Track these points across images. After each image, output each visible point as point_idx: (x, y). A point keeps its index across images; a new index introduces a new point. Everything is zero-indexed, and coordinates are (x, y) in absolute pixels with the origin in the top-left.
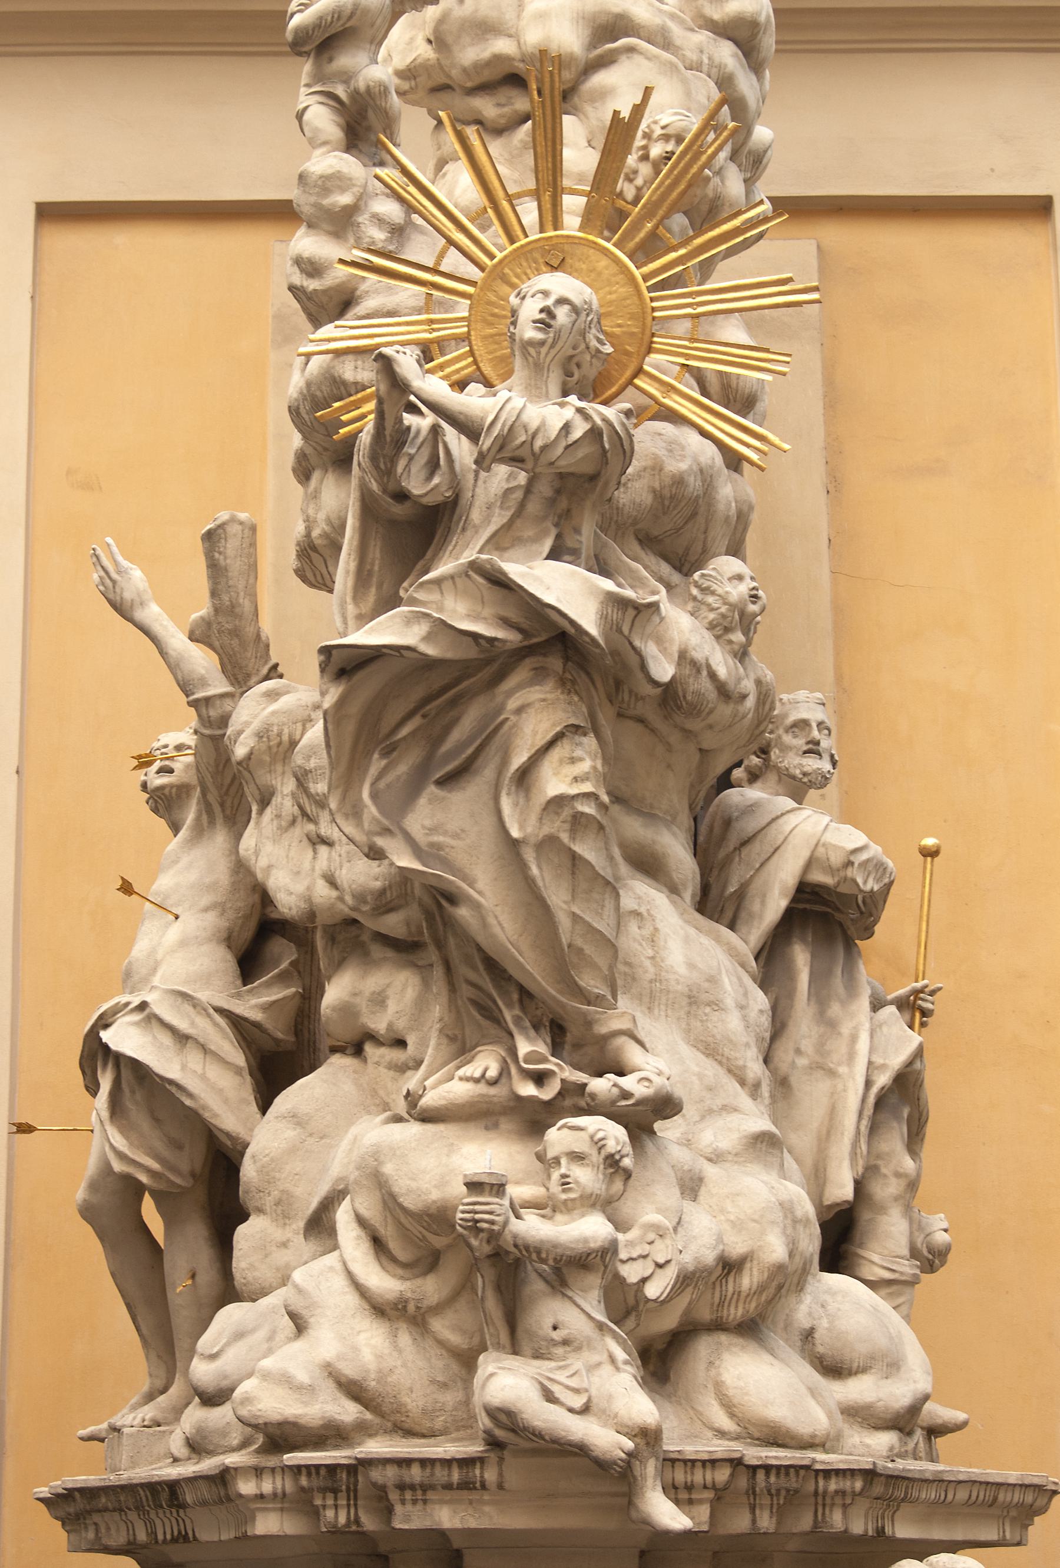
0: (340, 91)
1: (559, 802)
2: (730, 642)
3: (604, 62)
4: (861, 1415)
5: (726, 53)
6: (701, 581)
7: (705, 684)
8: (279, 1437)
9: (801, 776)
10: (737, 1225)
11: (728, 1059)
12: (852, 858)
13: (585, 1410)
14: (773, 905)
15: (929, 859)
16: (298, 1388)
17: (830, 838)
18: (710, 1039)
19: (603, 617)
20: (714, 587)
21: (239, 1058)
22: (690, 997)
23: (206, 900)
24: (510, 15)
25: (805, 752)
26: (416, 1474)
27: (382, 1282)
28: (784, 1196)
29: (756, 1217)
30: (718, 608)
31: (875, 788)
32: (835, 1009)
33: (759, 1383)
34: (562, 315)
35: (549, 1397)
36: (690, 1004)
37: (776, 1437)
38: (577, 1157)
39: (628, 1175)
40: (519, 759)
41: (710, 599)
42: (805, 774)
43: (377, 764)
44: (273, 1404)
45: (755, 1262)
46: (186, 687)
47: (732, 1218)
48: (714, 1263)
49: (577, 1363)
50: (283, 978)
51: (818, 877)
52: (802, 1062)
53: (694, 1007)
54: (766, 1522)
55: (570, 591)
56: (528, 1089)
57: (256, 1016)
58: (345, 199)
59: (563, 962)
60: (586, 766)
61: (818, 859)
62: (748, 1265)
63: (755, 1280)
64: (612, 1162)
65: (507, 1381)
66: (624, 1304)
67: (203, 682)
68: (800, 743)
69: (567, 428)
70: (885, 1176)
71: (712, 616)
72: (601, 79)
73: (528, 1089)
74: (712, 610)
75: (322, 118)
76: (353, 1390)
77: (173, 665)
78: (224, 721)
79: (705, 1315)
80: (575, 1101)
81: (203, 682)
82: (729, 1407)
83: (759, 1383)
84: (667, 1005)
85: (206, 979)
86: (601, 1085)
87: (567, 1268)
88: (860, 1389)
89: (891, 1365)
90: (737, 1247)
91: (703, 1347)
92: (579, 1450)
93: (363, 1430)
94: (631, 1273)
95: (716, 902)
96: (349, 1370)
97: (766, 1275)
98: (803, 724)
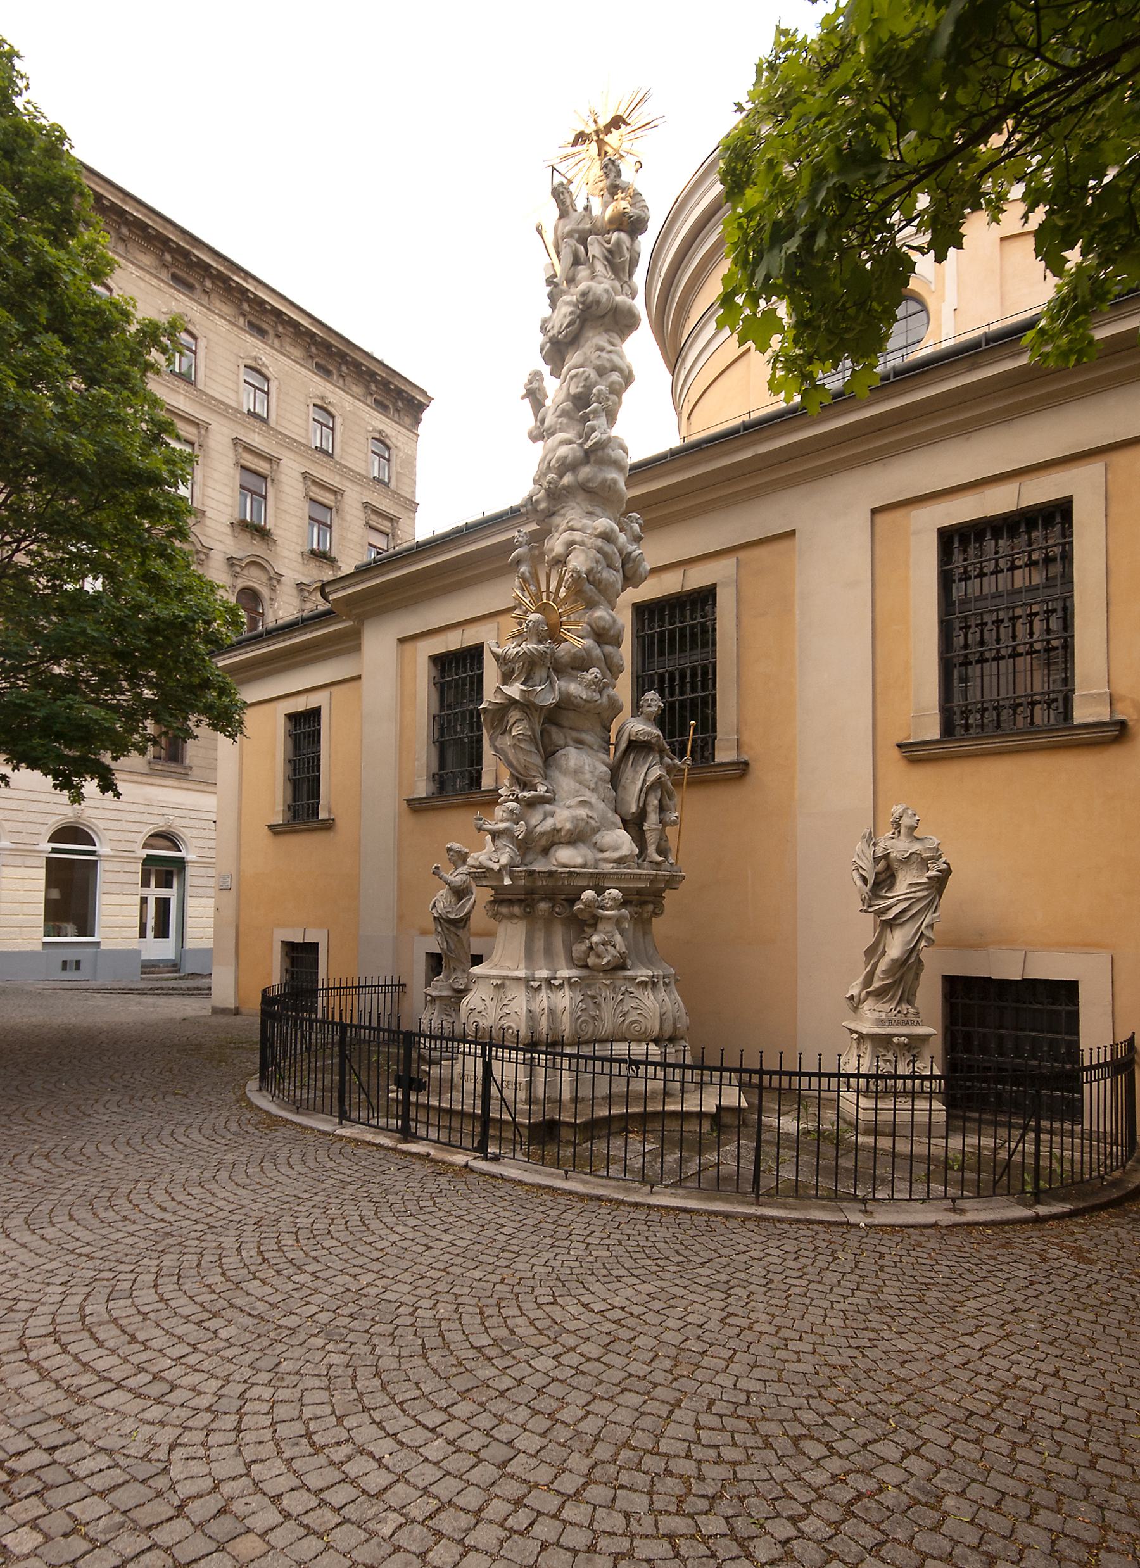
83: (567, 856)
88: (607, 855)
90: (559, 826)
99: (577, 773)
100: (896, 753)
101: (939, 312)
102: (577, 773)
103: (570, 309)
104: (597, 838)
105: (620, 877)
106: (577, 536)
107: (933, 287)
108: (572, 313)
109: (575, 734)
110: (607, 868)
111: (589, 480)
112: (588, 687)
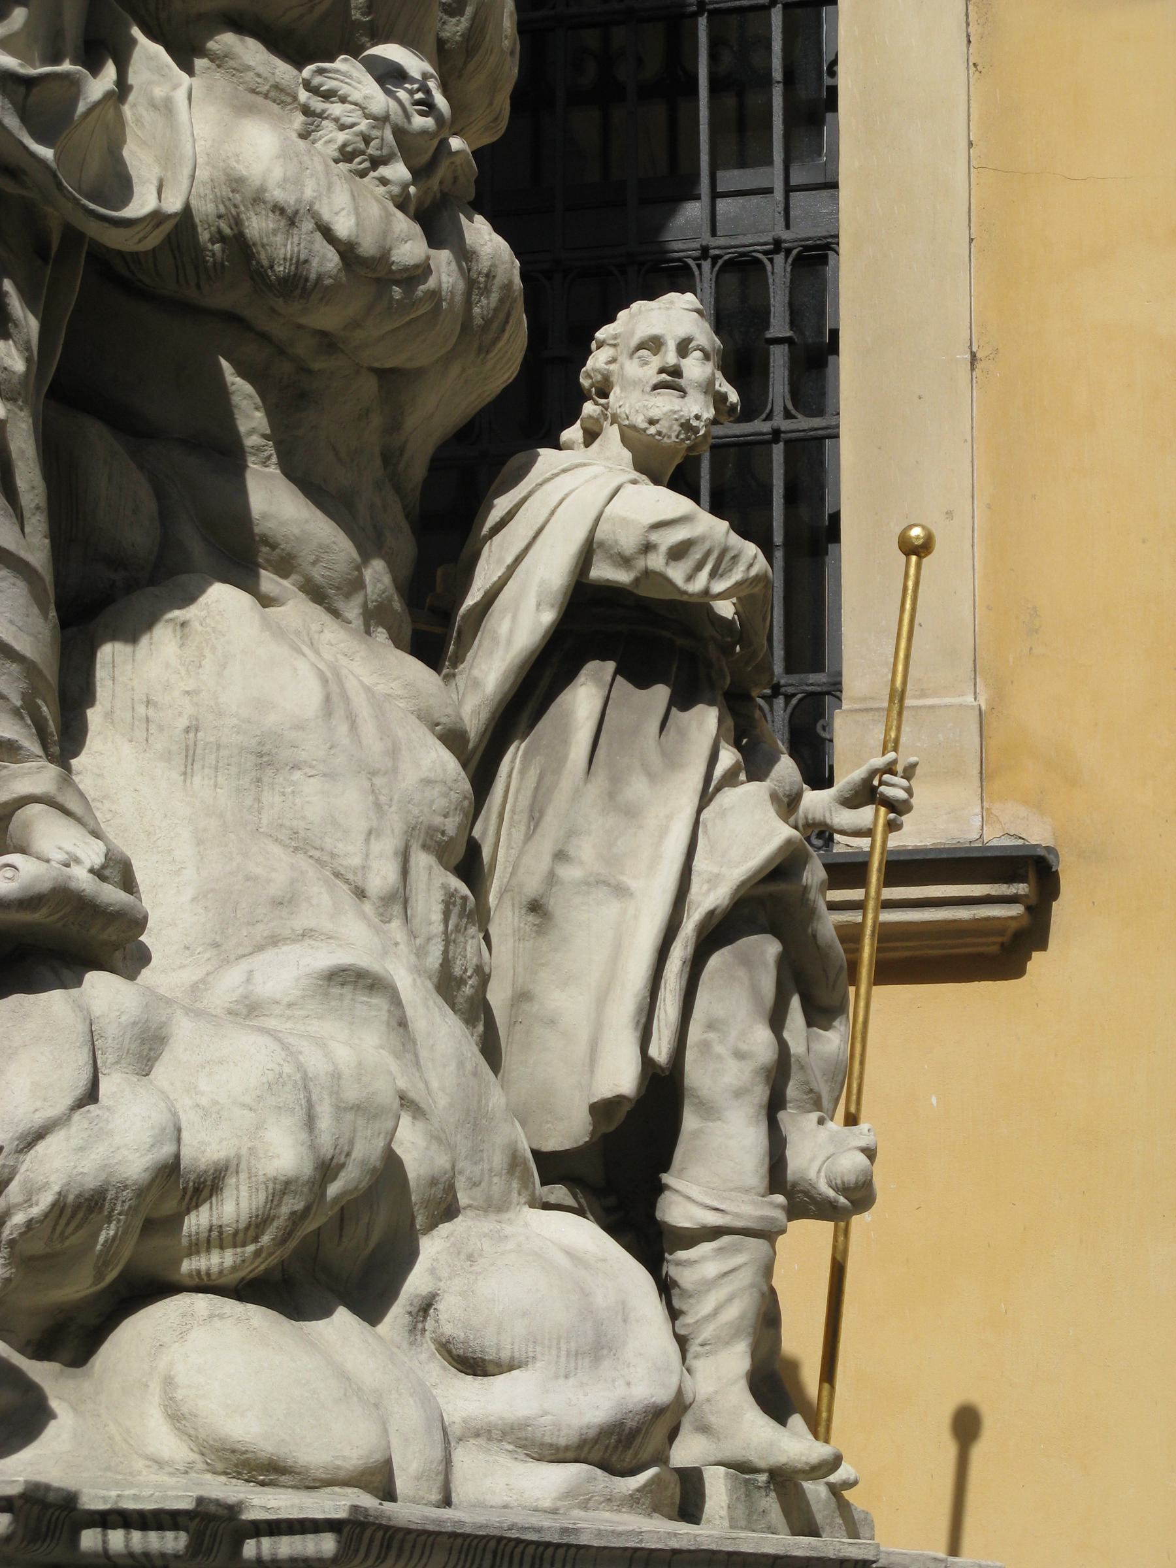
2: (384, 181)
6: (317, 80)
9: (644, 425)
11: (333, 855)
12: (654, 537)
14: (519, 611)
15: (914, 558)
18: (301, 824)
20: (344, 90)
22: (261, 755)
25: (656, 387)
29: (248, 1100)
30: (353, 125)
31: (1034, 497)
32: (638, 788)
36: (260, 766)
41: (336, 109)
42: (652, 422)
45: (243, 1176)
47: (204, 1101)
48: (146, 1176)
51: (602, 571)
53: (270, 772)
61: (601, 544)
62: (231, 1181)
63: (244, 1204)
68: (650, 373)
70: (719, 1057)
71: (342, 137)
74: (343, 127)
82: (176, 1417)
84: (216, 769)
90: (203, 1147)
97: (262, 1196)
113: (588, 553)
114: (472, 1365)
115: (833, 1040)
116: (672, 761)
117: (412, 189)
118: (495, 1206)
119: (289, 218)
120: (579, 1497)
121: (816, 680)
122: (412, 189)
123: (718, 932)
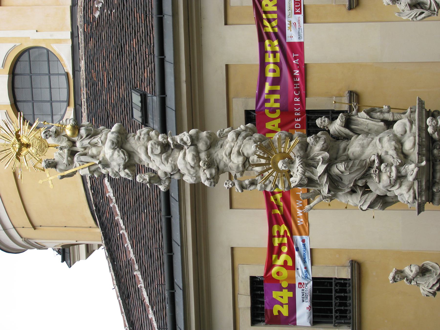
0: (248, 186)
1: (345, 169)
3: (243, 154)
4: (411, 129)
5: (240, 138)
7: (325, 145)
8: (415, 198)
10: (391, 147)
13: (413, 171)
14: (347, 131)
16: (409, 196)
17: (339, 124)
19: (324, 164)
21: (367, 195)
23: (346, 197)
24: (236, 165)
26: (419, 187)
27: (397, 186)
28: (387, 141)
32: (360, 123)
33: (409, 144)
34: (284, 165)
35: (412, 174)
37: (414, 144)
38: (386, 170)
39: (388, 164)
40: (340, 173)
43: (340, 187)
44: (411, 200)
46: (321, 201)
49: (408, 171)
50: (356, 188)
52: (366, 127)
54: (424, 149)
55: (321, 169)
56: (377, 172)
57: (362, 192)
58: (263, 186)
59: (362, 167)
60: (341, 166)
64: (386, 166)
65: (411, 178)
66: (402, 165)
67: (321, 199)
68: (324, 123)
69: (301, 167)
72: (246, 154)
73: (377, 172)
75: (252, 188)
76: (409, 190)
77: (318, 202)
78: (325, 197)
79: (401, 150)
80: (379, 168)
81: (321, 199)
82: (411, 149)
83: (409, 144)
85: (357, 198)
86: (376, 164)
87: (398, 171)
88: (408, 129)
89: (405, 125)
90: (393, 148)
91: (404, 151)
92: (417, 172)
93: (414, 189)
94: (398, 164)
95: (347, 138)
96: (407, 190)
98: (321, 122)
99: (363, 147)
100: (353, 12)
101: (35, 40)
102: (363, 147)
103: (116, 152)
104: (399, 135)
105: (420, 120)
106: (235, 150)
107: (17, 44)
108: (118, 152)
109: (341, 151)
110: (415, 128)
111: (206, 144)
112: (317, 142)
113: (342, 126)
114: (406, 132)
115: (377, 108)
116: (357, 120)
117: (438, 147)
118: (394, 131)
119: (323, 146)
120: (415, 125)
121: (330, 112)
122: (438, 147)
123: (371, 117)
